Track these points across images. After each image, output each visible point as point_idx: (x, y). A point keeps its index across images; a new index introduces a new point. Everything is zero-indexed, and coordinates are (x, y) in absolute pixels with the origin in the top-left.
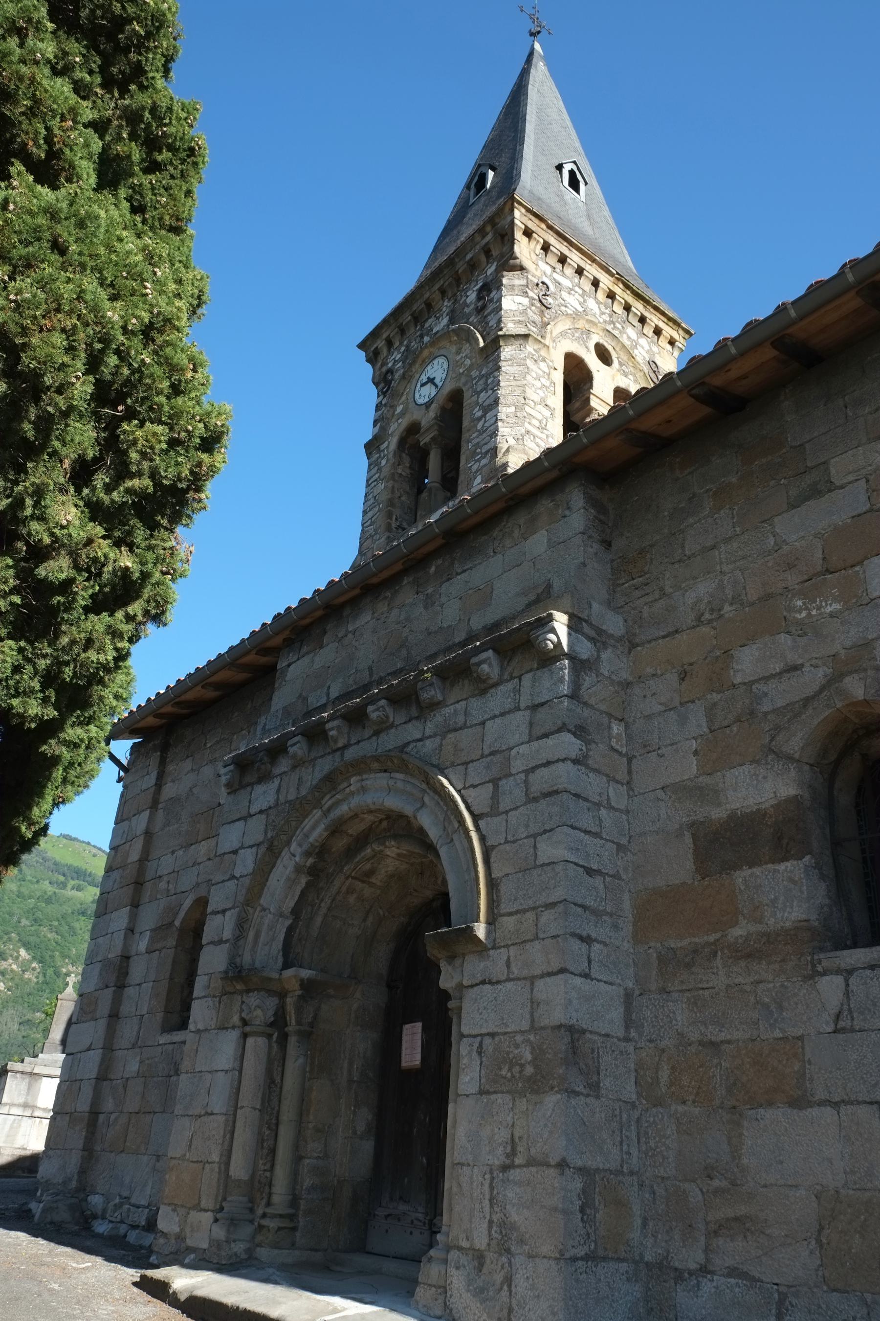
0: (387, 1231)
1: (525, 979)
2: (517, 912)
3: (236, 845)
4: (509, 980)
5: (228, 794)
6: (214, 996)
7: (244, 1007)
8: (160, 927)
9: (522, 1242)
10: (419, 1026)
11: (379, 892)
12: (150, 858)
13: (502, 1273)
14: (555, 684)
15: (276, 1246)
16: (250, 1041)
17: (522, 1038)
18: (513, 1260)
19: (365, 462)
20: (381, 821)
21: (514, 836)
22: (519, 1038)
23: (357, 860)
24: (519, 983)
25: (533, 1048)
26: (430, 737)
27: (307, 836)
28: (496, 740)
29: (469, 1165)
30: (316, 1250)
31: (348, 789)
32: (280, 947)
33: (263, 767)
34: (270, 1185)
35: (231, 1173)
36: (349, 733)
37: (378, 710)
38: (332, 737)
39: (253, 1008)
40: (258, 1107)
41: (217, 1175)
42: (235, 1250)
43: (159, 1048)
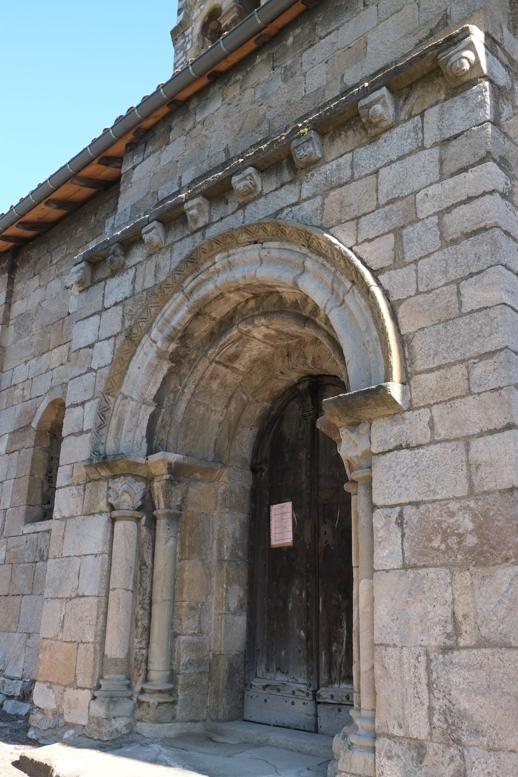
0: (266, 701)
1: (456, 439)
2: (439, 368)
3: (91, 339)
4: (433, 442)
5: (80, 292)
6: (78, 484)
7: (110, 492)
8: (18, 430)
9: (477, 732)
10: (288, 506)
11: (241, 377)
12: (4, 370)
13: (452, 766)
14: (472, 111)
15: (157, 721)
16: (119, 525)
17: (458, 505)
18: (466, 753)
19: (172, 50)
20: (247, 301)
21: (427, 286)
22: (453, 506)
23: (221, 343)
24: (448, 445)
25: (475, 515)
26: (309, 198)
27: (168, 321)
28: (395, 187)
29: (395, 646)
30: (196, 721)
31: (212, 268)
32: (144, 433)
33: (116, 259)
34: (147, 662)
35: (107, 652)
36: (210, 212)
37: (244, 178)
38: (192, 216)
39: (120, 493)
40: (131, 588)
41: (93, 654)
42: (116, 726)
43: (24, 537)
